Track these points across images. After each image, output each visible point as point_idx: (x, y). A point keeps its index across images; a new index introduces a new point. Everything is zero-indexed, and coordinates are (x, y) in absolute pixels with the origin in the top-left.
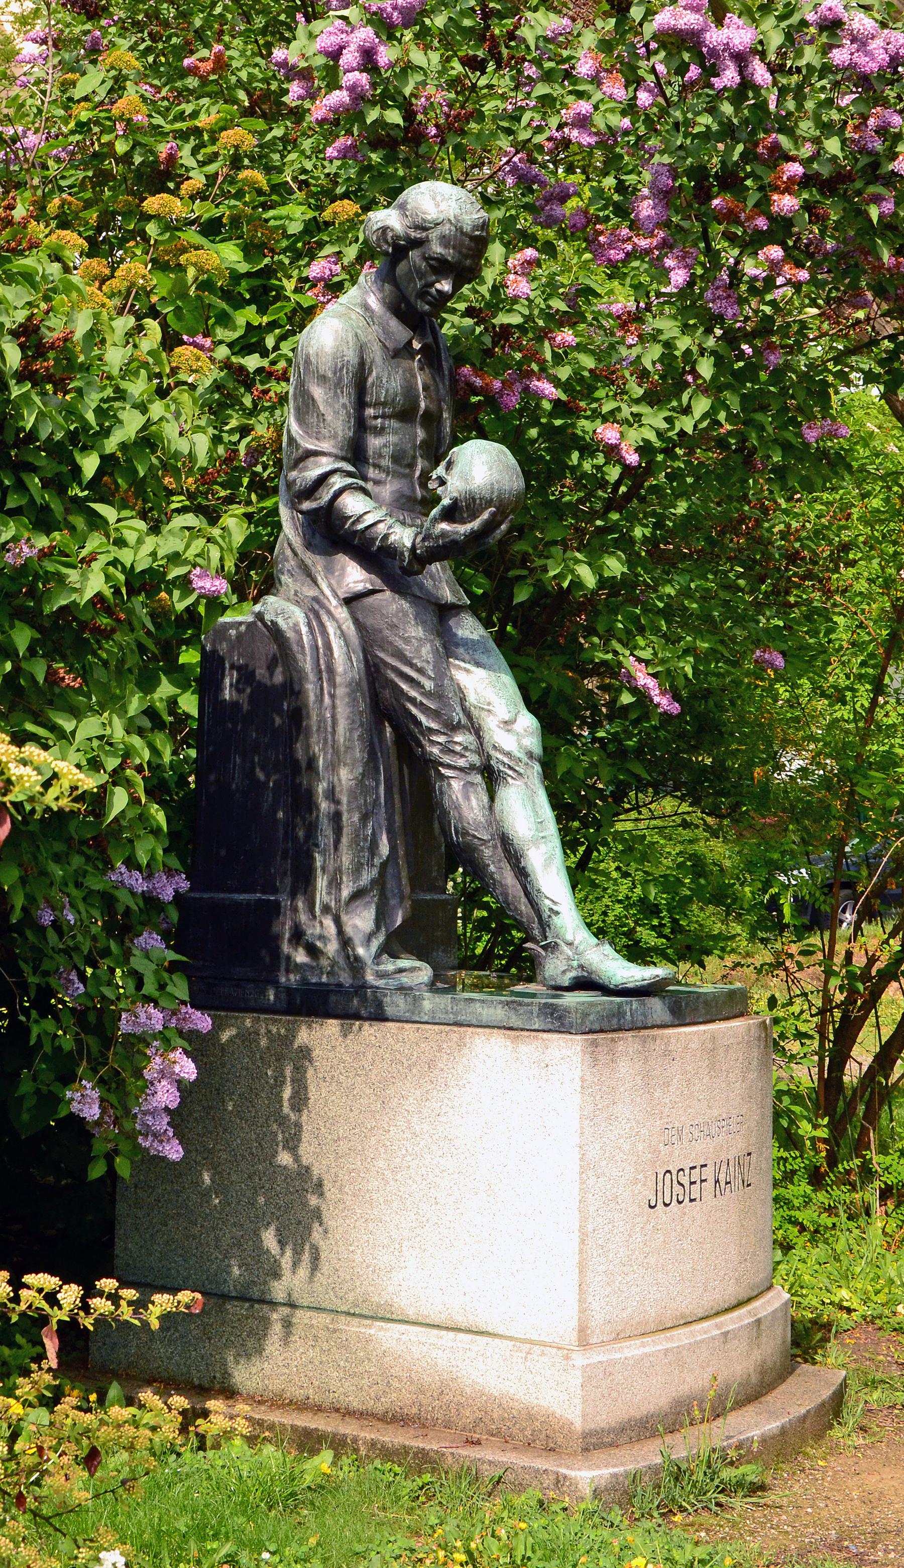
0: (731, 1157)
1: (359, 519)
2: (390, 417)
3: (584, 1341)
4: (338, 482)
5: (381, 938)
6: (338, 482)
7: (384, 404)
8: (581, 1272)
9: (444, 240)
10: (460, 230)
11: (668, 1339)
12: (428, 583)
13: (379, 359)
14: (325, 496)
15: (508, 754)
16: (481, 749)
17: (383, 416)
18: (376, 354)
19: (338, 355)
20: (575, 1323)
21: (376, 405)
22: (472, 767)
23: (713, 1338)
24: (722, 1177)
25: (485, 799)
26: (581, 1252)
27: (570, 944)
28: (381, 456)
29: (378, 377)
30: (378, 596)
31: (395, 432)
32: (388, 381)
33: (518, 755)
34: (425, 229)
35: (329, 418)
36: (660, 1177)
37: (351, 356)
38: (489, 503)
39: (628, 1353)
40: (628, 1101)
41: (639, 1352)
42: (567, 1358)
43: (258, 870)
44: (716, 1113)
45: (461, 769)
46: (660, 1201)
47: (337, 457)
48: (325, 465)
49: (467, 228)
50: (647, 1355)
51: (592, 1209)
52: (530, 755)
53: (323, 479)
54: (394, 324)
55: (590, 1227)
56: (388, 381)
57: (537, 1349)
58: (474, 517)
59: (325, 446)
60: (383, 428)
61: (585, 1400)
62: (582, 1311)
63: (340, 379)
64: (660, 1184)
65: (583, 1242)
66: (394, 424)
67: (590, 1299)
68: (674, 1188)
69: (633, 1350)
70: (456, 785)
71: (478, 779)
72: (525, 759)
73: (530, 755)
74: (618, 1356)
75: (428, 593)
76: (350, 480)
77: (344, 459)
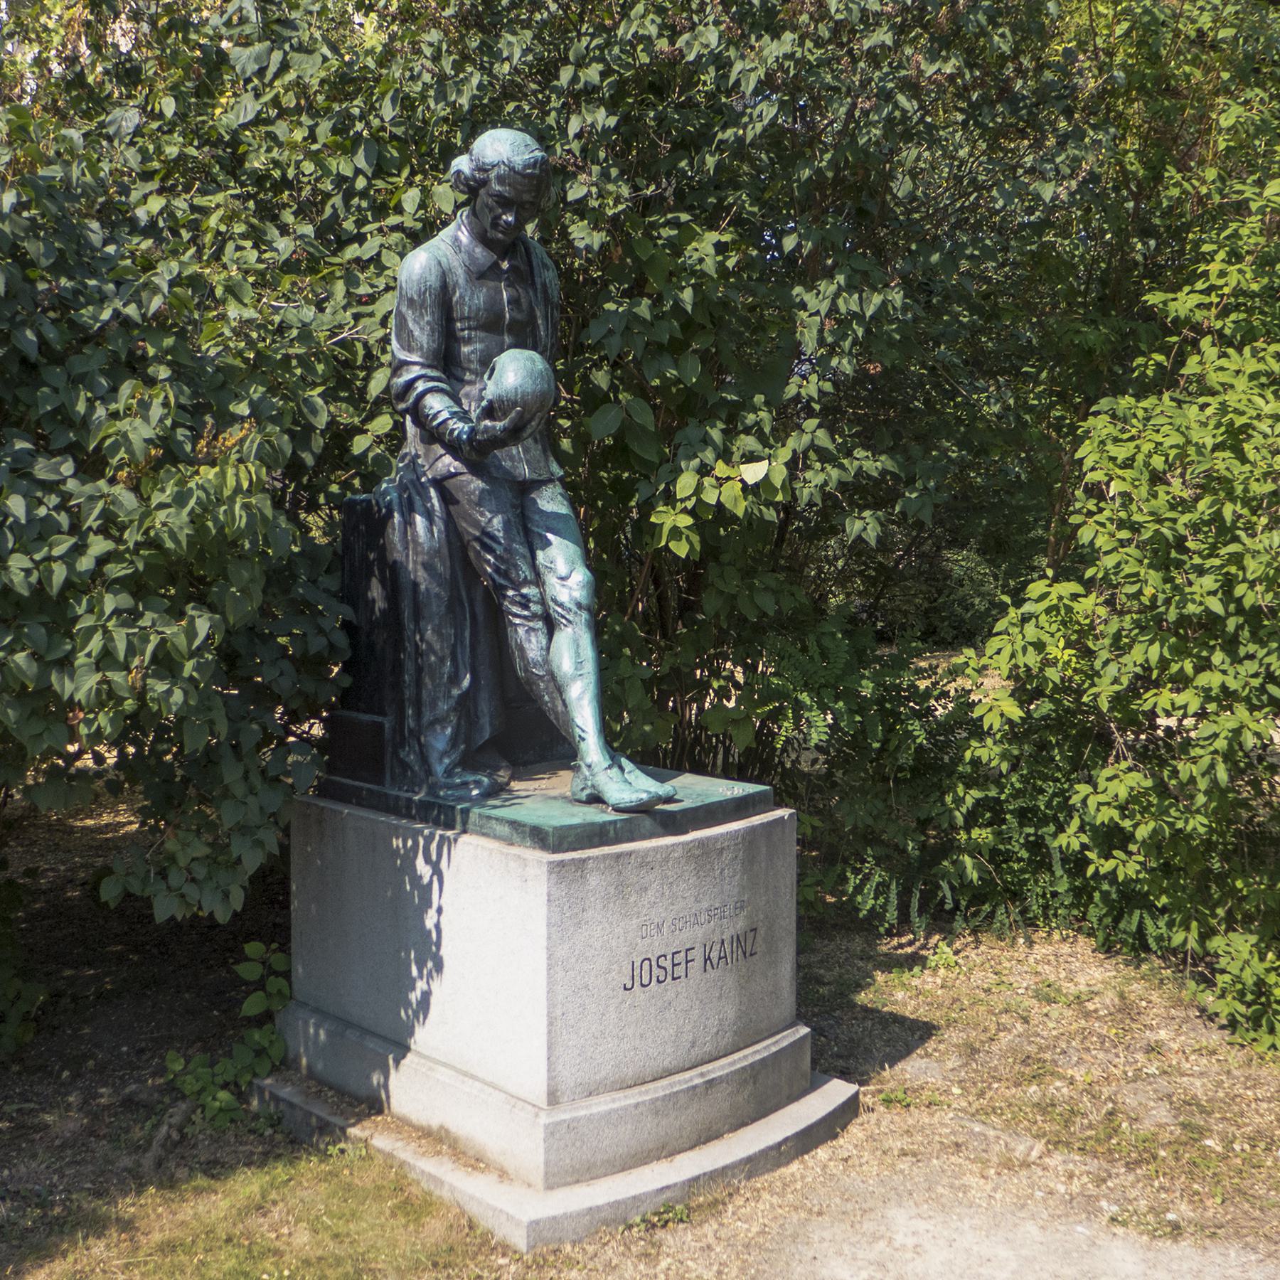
0: (726, 936)
1: (435, 416)
2: (475, 329)
3: (553, 1098)
4: (420, 386)
5: (455, 756)
6: (420, 386)
7: (469, 318)
8: (549, 1048)
9: (500, 179)
10: (512, 169)
11: (640, 1093)
12: (507, 464)
13: (461, 281)
14: (412, 398)
15: (561, 605)
16: (542, 602)
17: (469, 328)
18: (460, 275)
19: (423, 280)
20: (544, 1089)
21: (462, 319)
22: (534, 616)
23: (695, 1087)
24: (714, 955)
25: (544, 642)
26: (549, 1032)
27: (589, 766)
28: (470, 361)
29: (461, 297)
30: (463, 478)
31: (481, 341)
32: (471, 299)
33: (568, 605)
34: (486, 171)
35: (416, 333)
36: (637, 965)
37: (433, 280)
38: (515, 404)
39: (595, 1110)
40: (599, 907)
41: (603, 1108)
42: (537, 1115)
43: (363, 695)
44: (705, 905)
45: (525, 617)
46: (637, 984)
47: (423, 365)
48: (416, 371)
49: (519, 167)
50: (616, 1110)
51: (560, 998)
52: (579, 605)
53: (410, 385)
54: (479, 251)
55: (559, 1012)
56: (471, 299)
57: (520, 1104)
58: (505, 415)
59: (415, 358)
60: (470, 338)
61: (547, 1151)
62: (551, 1078)
63: (424, 301)
64: (637, 972)
65: (550, 1024)
66: (481, 334)
67: (560, 1068)
68: (657, 971)
69: (603, 1104)
70: (521, 631)
71: (540, 624)
72: (574, 608)
73: (579, 605)
74: (582, 1113)
75: (507, 472)
76: (431, 384)
77: (429, 366)
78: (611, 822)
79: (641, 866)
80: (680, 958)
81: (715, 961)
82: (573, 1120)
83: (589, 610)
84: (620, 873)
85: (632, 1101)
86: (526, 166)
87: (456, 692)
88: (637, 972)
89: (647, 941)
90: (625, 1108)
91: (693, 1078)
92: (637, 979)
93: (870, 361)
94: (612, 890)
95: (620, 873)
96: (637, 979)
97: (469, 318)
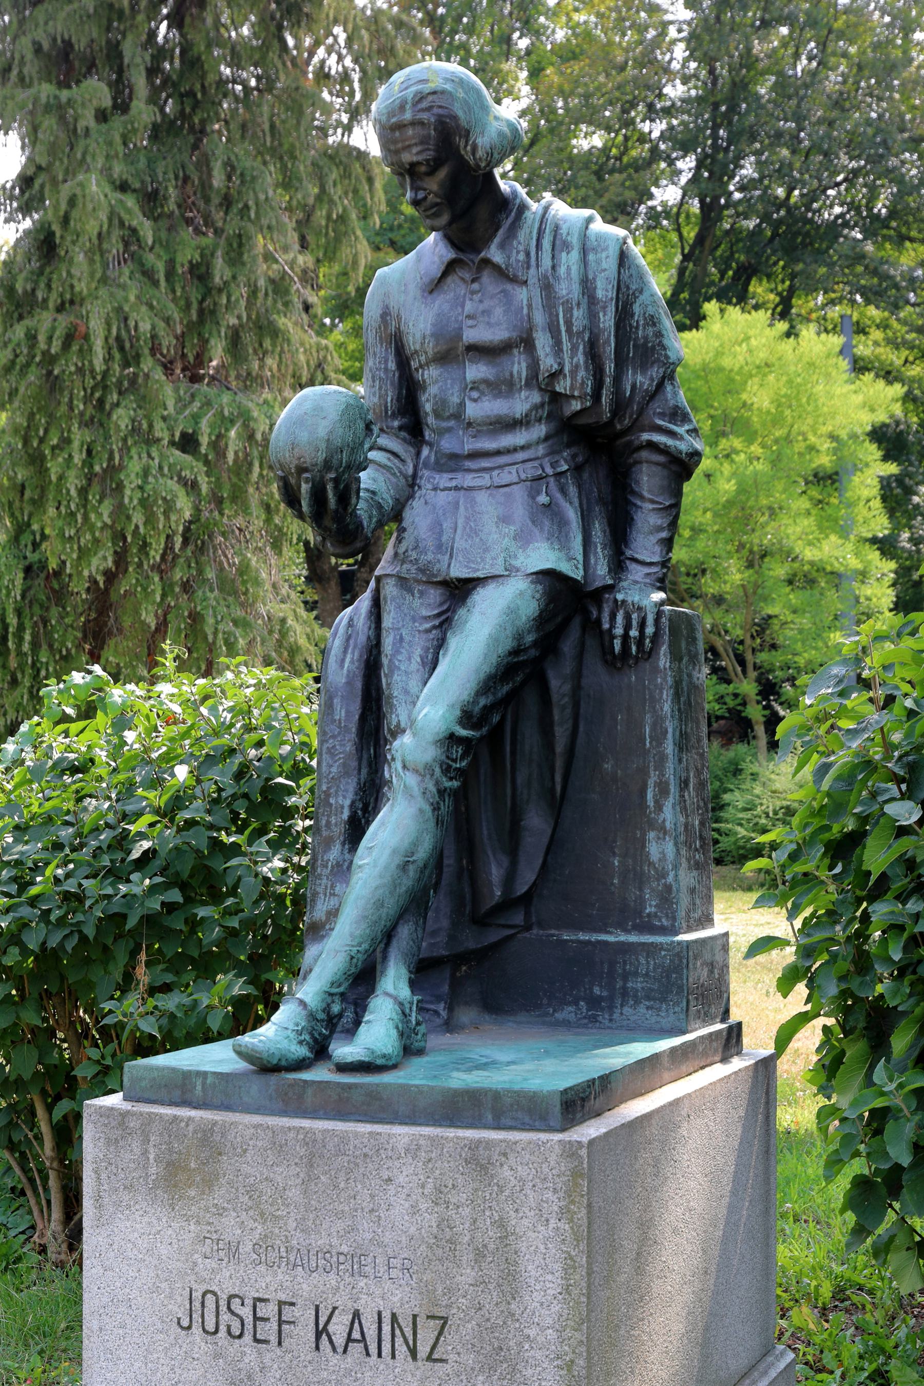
36: (197, 1295)
80: (269, 1310)
88: (197, 1304)
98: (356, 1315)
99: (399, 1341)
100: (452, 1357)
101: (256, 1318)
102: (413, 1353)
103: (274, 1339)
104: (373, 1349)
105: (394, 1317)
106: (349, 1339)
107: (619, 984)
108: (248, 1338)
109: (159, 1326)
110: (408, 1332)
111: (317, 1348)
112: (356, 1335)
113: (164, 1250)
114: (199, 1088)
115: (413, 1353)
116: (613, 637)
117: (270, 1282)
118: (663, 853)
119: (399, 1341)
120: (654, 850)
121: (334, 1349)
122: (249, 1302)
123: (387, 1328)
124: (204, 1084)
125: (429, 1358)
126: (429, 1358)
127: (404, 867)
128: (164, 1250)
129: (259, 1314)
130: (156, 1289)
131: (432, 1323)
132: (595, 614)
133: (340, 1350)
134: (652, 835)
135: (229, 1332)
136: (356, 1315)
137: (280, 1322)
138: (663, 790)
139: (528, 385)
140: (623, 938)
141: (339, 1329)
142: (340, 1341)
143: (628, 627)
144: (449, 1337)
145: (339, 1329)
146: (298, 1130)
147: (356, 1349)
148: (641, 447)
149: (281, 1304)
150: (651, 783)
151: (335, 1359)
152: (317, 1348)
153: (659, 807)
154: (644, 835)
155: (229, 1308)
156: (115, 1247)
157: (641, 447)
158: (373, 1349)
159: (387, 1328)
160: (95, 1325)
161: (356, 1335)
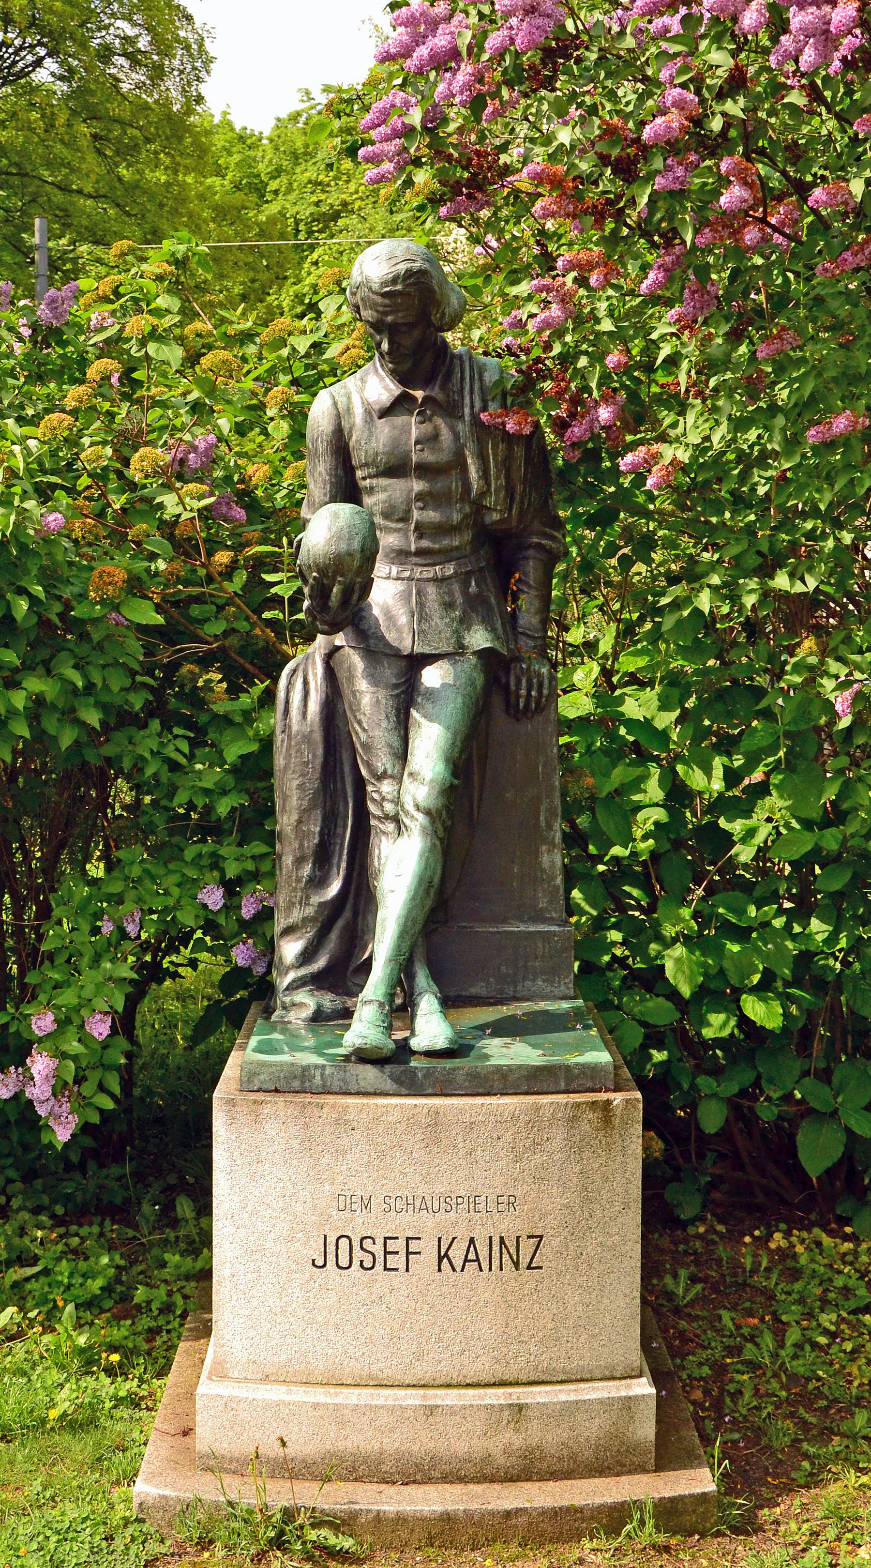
11: (326, 1394)
36: (331, 1240)
49: (376, 287)
64: (331, 1248)
78: (316, 1067)
79: (337, 1122)
80: (398, 1245)
81: (458, 1263)
82: (231, 1399)
83: (428, 813)
84: (306, 1126)
85: (312, 1399)
86: (385, 284)
87: (315, 900)
88: (331, 1248)
89: (347, 1214)
90: (301, 1405)
91: (413, 1398)
92: (331, 1257)
93: (817, 466)
94: (295, 1143)
95: (306, 1126)
96: (331, 1257)
97: (366, 465)
98: (472, 1241)
99: (506, 1257)
100: (545, 1265)
101: (386, 1253)
102: (516, 1265)
103: (402, 1266)
104: (485, 1265)
105: (502, 1239)
106: (466, 1260)
107: (521, 963)
108: (379, 1267)
109: (294, 1267)
110: (513, 1250)
111: (440, 1270)
112: (472, 1256)
113: (299, 1208)
114: (318, 1078)
115: (516, 1265)
116: (518, 696)
117: (403, 1224)
118: (553, 862)
119: (506, 1257)
120: (545, 859)
121: (454, 1270)
122: (380, 1241)
123: (496, 1248)
124: (322, 1075)
125: (529, 1267)
126: (529, 1267)
127: (427, 892)
128: (299, 1208)
129: (389, 1249)
130: (291, 1239)
131: (532, 1240)
132: (504, 680)
133: (459, 1269)
134: (544, 848)
135: (362, 1266)
136: (472, 1241)
137: (408, 1253)
138: (552, 813)
139: (462, 500)
140: (522, 928)
141: (457, 1254)
142: (458, 1263)
143: (529, 690)
144: (542, 1250)
145: (457, 1254)
146: (401, 1106)
147: (472, 1267)
148: (530, 546)
149: (408, 1239)
150: (543, 808)
151: (453, 1276)
152: (440, 1270)
153: (550, 827)
154: (537, 849)
155: (362, 1248)
156: (249, 1209)
157: (530, 546)
158: (485, 1265)
159: (496, 1248)
160: (227, 1272)
161: (472, 1256)
